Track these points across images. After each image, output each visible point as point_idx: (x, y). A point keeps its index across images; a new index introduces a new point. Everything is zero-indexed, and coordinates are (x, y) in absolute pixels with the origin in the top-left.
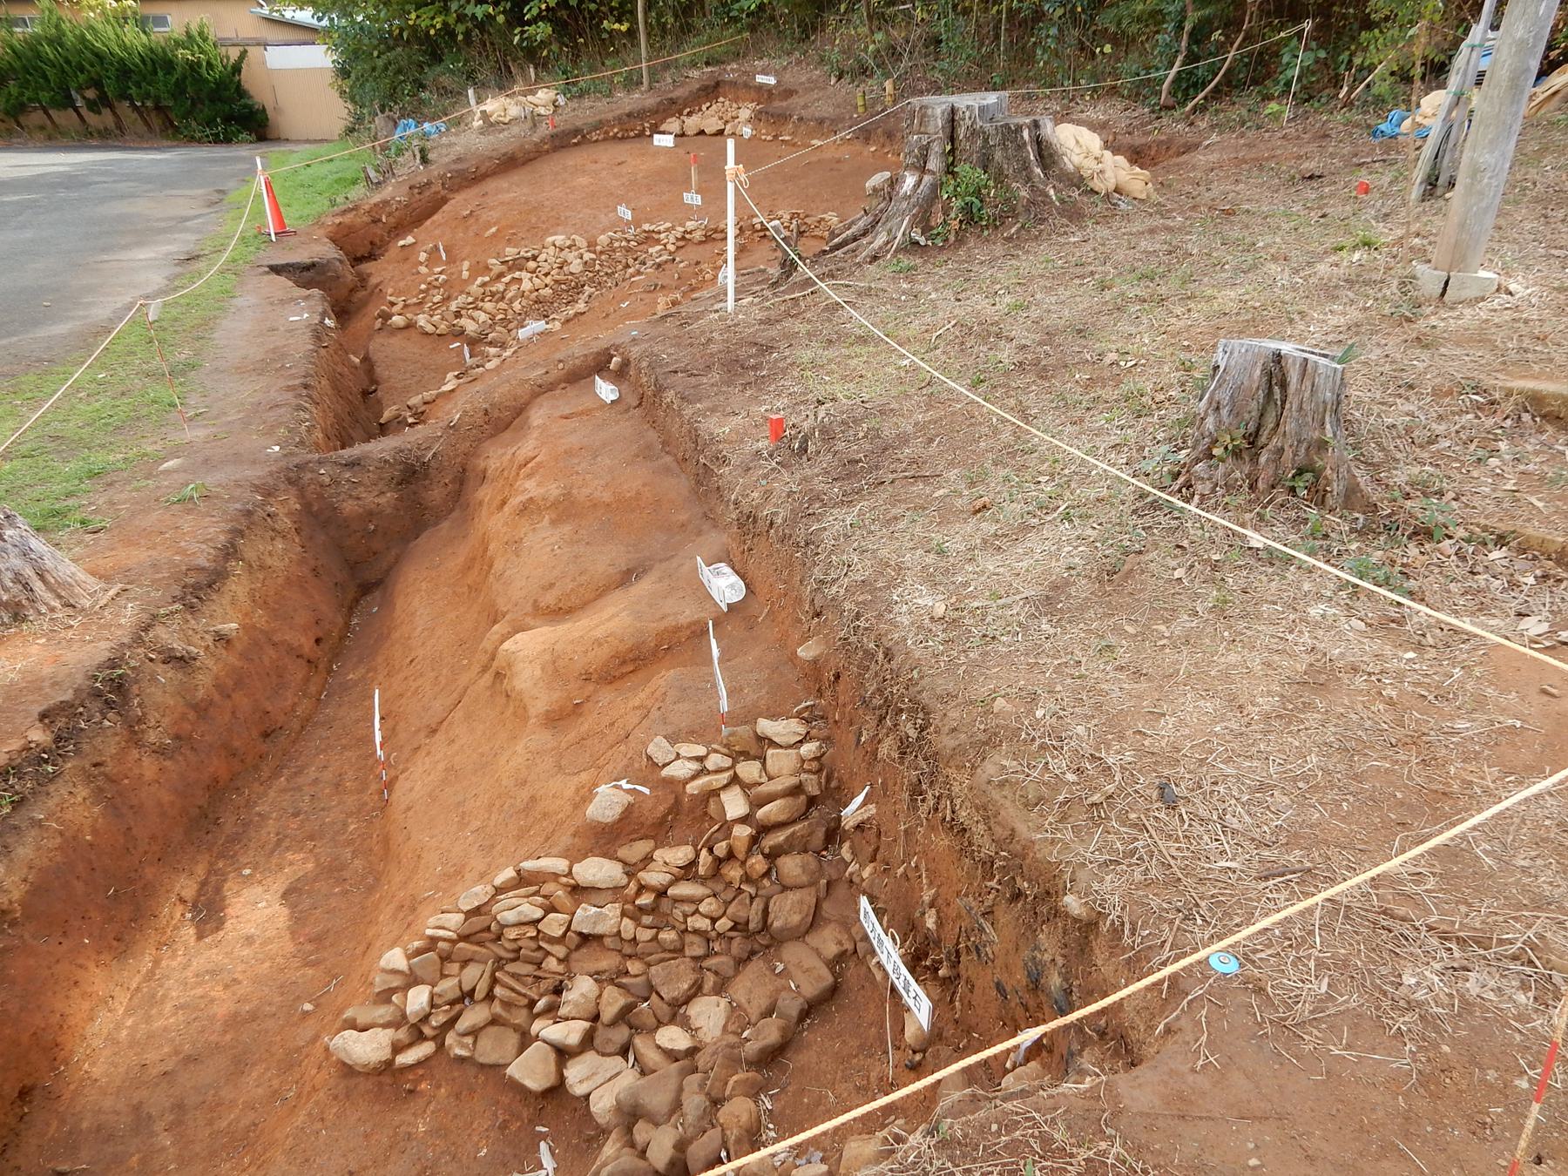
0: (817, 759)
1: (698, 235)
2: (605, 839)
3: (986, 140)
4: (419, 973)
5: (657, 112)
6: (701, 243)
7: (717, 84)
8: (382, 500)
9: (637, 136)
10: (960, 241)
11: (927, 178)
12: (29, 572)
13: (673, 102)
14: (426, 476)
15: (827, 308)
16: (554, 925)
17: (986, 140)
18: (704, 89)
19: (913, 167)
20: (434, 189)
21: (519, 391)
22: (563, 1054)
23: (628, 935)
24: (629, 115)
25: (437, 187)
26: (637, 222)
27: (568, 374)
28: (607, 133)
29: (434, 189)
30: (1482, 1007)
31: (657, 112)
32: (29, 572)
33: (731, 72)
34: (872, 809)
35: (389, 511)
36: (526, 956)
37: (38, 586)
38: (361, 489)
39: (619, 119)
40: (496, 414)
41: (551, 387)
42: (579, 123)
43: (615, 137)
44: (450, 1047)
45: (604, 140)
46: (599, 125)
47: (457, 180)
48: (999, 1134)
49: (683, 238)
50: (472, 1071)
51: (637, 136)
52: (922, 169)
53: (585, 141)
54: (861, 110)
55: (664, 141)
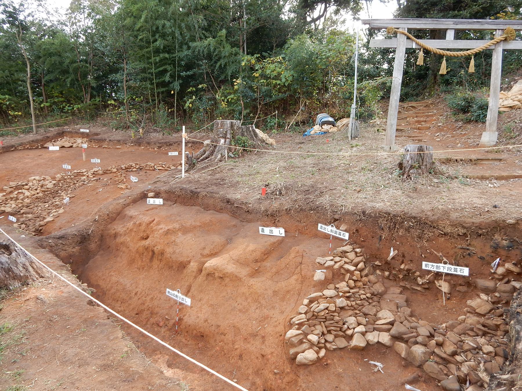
1: (101, 172)
2: (323, 284)
3: (242, 130)
4: (306, 332)
5: (42, 141)
6: (102, 174)
8: (74, 250)
10: (243, 156)
11: (227, 140)
12: (28, 264)
13: (48, 137)
14: (89, 239)
16: (332, 307)
17: (242, 130)
18: (58, 134)
19: (223, 137)
21: (118, 207)
22: (363, 334)
23: (350, 305)
24: (32, 141)
26: (72, 169)
27: (133, 200)
28: (24, 147)
31: (42, 141)
32: (28, 264)
33: (66, 128)
34: (396, 252)
35: (77, 254)
36: (329, 318)
37: (30, 269)
38: (66, 246)
39: (29, 142)
40: (111, 215)
41: (128, 205)
42: (13, 143)
43: (28, 149)
44: (330, 347)
45: (24, 149)
46: (21, 144)
49: (94, 174)
50: (339, 352)
52: (225, 138)
53: (16, 149)
54: (133, 137)
55: (53, 148)
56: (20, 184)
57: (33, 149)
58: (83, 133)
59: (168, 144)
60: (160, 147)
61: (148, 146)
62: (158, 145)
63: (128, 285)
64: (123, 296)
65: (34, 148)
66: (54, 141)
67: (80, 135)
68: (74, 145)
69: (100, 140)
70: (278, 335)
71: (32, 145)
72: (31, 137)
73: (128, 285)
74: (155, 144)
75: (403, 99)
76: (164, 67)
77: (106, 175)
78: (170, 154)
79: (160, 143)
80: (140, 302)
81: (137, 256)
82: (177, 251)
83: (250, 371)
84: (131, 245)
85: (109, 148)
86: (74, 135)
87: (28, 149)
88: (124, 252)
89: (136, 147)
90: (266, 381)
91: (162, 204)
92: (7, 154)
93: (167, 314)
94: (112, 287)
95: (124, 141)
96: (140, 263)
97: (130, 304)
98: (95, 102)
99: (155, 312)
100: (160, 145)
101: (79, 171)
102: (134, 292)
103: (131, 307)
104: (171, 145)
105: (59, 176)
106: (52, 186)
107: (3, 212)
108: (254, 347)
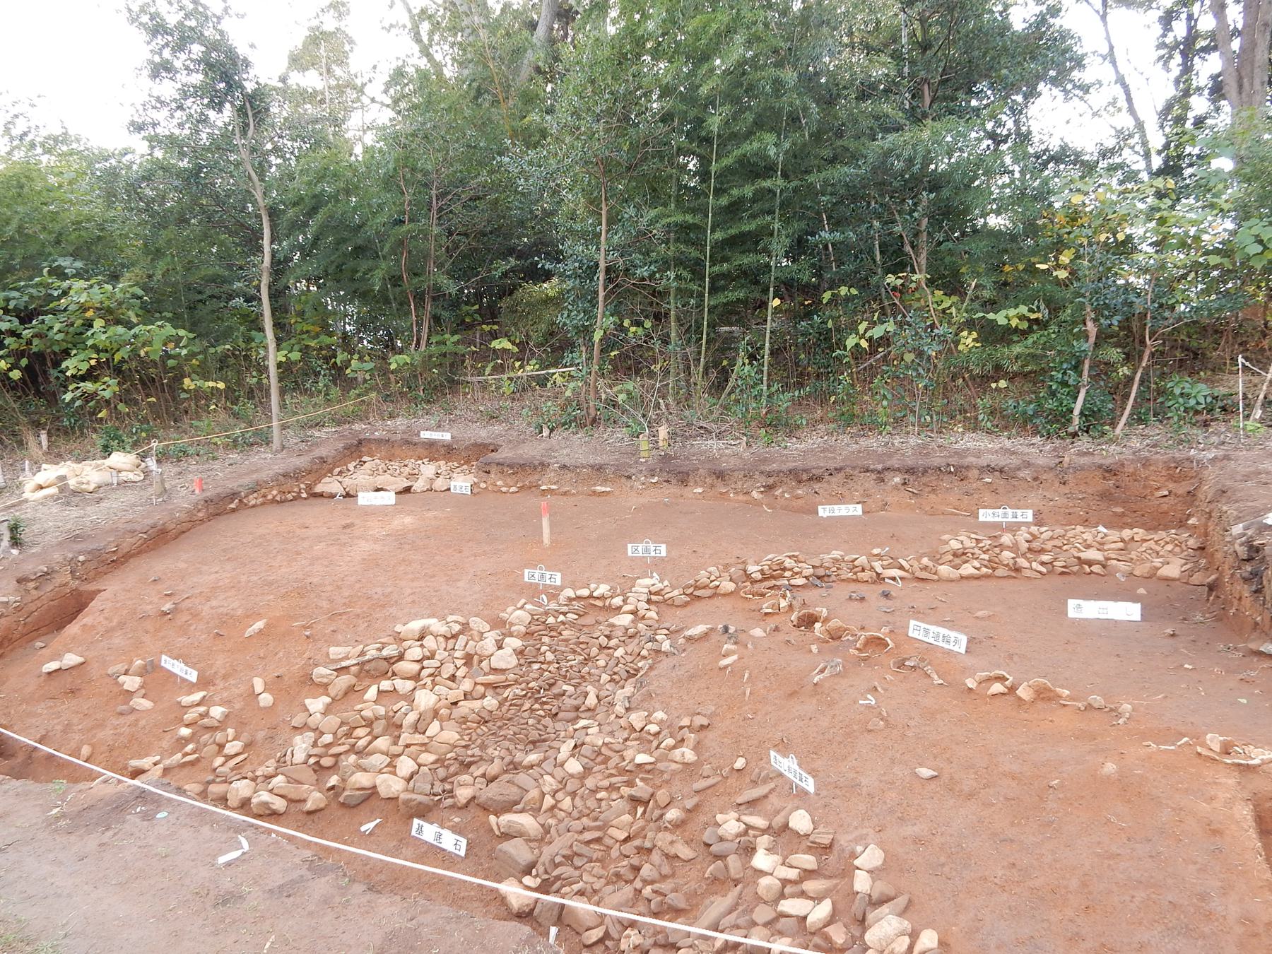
0: (142, 687)
5: (310, 472)
6: (686, 604)
7: (360, 442)
9: (294, 499)
13: (323, 460)
15: (258, 433)
20: (59, 580)
25: (64, 577)
28: (264, 496)
29: (59, 580)
30: (144, 420)
31: (310, 472)
39: (275, 478)
42: (232, 485)
43: (273, 501)
47: (92, 566)
48: (1215, 267)
51: (294, 499)
56: (372, 653)
57: (286, 501)
58: (431, 444)
59: (805, 477)
60: (770, 488)
61: (719, 483)
62: (763, 480)
65: (290, 496)
66: (340, 473)
67: (420, 450)
68: (419, 486)
69: (523, 466)
71: (284, 488)
72: (266, 463)
74: (748, 476)
75: (282, 392)
76: (759, 221)
77: (698, 606)
78: (824, 511)
79: (769, 475)
85: (565, 494)
86: (397, 451)
87: (273, 501)
89: (674, 489)
92: (223, 524)
95: (618, 468)
98: (443, 349)
100: (771, 481)
101: (585, 592)
104: (819, 479)
105: (519, 616)
106: (514, 661)
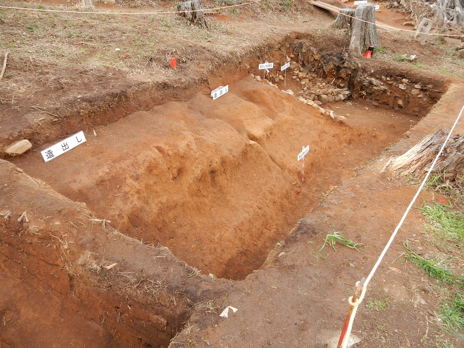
63: (246, 215)
64: (258, 224)
70: (325, 124)
73: (246, 215)
80: (271, 205)
81: (196, 199)
82: (230, 147)
83: (338, 146)
84: (176, 198)
88: (175, 218)
90: (346, 141)
91: (84, 140)
93: (291, 183)
94: (241, 239)
96: (206, 201)
97: (271, 218)
99: (285, 193)
102: (257, 210)
103: (274, 216)
107: (463, 69)
108: (328, 138)
